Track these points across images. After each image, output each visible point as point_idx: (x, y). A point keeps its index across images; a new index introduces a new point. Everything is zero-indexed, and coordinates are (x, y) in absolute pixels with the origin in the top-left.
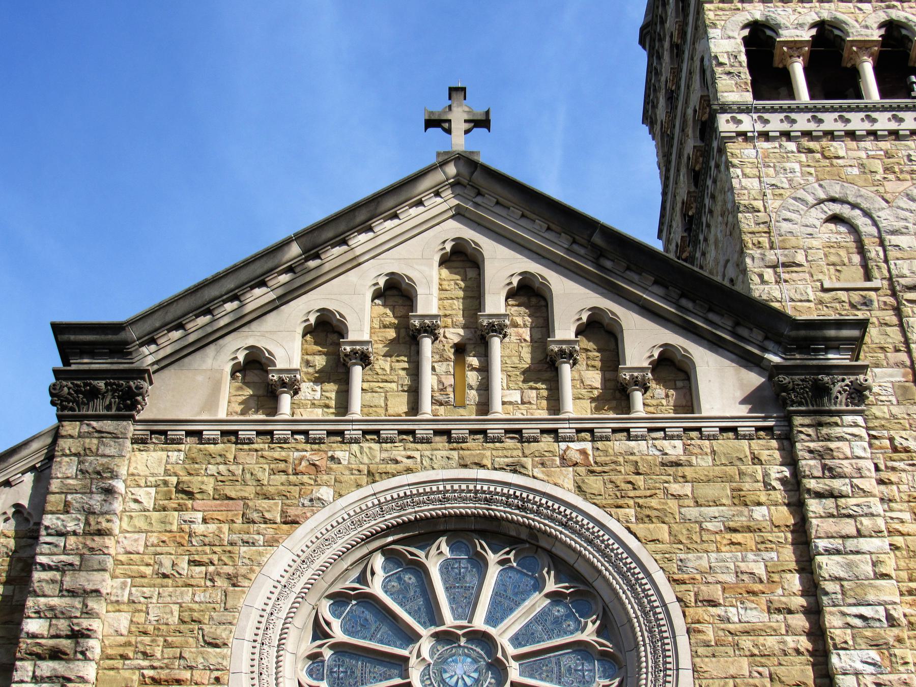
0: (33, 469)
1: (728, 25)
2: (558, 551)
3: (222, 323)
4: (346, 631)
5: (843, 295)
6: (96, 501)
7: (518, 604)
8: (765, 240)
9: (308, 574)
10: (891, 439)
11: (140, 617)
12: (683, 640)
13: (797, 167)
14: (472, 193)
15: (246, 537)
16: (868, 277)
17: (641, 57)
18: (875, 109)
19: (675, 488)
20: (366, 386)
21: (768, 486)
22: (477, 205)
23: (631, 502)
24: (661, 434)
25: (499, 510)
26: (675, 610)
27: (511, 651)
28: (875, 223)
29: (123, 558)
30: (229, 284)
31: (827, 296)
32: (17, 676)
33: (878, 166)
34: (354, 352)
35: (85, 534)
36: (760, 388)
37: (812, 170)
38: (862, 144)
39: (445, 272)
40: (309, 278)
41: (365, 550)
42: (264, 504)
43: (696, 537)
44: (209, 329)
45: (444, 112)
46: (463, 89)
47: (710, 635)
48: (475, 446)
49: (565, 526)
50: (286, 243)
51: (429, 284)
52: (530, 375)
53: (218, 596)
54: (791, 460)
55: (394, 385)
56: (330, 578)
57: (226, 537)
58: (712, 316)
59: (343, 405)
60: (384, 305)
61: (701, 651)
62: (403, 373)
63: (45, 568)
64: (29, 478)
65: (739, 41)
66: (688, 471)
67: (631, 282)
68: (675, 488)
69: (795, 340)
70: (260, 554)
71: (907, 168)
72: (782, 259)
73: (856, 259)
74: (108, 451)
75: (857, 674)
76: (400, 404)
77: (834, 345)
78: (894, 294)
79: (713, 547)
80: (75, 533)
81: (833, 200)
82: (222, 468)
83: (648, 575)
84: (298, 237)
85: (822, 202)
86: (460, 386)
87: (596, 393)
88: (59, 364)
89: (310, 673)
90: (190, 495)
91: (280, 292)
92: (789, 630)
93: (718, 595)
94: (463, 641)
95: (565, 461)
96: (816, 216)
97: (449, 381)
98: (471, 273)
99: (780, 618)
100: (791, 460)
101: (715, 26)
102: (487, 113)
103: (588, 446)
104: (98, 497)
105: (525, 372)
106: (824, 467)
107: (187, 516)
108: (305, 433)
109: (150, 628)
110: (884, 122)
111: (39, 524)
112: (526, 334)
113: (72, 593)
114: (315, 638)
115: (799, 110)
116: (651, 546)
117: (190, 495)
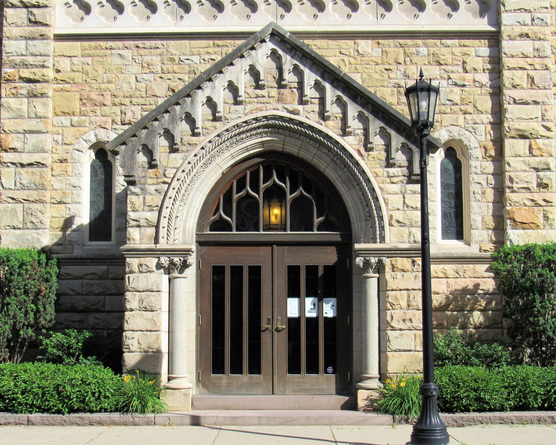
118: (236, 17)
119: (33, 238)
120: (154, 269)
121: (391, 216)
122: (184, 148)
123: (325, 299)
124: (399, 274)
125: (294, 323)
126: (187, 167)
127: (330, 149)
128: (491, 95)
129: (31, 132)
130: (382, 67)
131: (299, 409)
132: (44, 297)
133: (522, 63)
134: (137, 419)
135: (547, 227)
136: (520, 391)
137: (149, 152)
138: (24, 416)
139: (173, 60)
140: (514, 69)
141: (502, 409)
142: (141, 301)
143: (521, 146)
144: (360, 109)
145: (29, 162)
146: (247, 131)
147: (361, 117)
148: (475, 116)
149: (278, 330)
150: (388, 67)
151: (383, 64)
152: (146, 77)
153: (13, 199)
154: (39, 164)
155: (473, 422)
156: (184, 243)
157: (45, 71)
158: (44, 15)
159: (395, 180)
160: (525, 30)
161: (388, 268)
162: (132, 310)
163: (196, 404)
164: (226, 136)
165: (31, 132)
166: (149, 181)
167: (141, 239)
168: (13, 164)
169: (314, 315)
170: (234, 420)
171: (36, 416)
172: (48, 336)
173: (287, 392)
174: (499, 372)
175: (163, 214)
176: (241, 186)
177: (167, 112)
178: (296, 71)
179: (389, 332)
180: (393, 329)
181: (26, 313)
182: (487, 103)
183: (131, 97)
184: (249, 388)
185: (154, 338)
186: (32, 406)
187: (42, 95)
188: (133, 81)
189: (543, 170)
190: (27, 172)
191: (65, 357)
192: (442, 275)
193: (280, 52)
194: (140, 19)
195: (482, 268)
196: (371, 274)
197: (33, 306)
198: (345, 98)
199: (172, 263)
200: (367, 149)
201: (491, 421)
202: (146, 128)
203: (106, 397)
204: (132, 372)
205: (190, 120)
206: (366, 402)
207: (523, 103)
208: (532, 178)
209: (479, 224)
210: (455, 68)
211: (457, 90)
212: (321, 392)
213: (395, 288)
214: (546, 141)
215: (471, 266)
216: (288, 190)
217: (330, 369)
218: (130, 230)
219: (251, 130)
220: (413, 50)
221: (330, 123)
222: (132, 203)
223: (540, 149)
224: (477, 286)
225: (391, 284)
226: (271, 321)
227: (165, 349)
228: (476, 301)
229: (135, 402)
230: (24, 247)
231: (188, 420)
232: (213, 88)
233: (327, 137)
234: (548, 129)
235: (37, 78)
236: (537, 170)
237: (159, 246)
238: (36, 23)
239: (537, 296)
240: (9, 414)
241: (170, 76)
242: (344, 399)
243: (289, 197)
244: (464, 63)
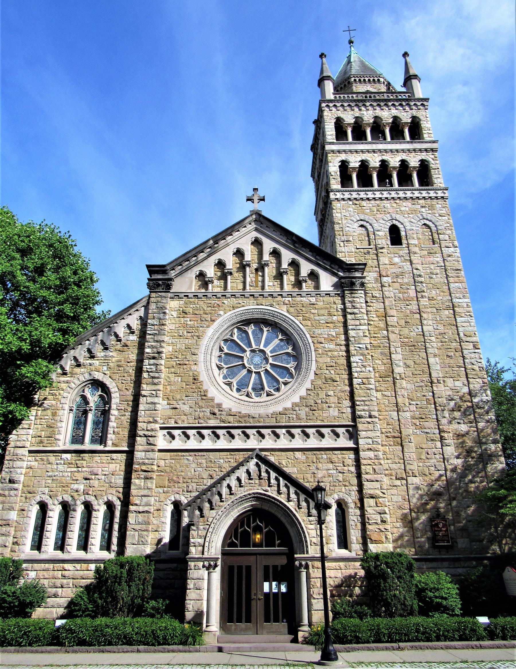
0: (144, 306)
1: (335, 162)
2: (282, 328)
3: (192, 263)
4: (228, 350)
5: (362, 250)
6: (161, 316)
7: (272, 342)
8: (341, 233)
9: (218, 335)
10: (372, 294)
11: (175, 347)
12: (313, 353)
13: (352, 209)
14: (260, 223)
15: (201, 325)
16: (370, 245)
17: (311, 154)
19: (313, 311)
20: (231, 281)
21: (337, 311)
22: (261, 227)
23: (301, 315)
24: (309, 296)
25: (267, 317)
26: (312, 344)
27: (270, 355)
28: (373, 228)
29: (169, 331)
30: (194, 252)
31: (358, 250)
32: (144, 364)
33: (375, 209)
34: (228, 272)
35: (160, 325)
36: (337, 282)
37: (356, 211)
38: (371, 202)
39: (252, 247)
40: (215, 250)
41: (232, 328)
42: (205, 316)
43: (318, 325)
44: (189, 266)
45: (252, 196)
46: (257, 189)
47: (320, 352)
48: (260, 298)
49: (284, 321)
50: (208, 241)
51: (248, 251)
52: (275, 278)
53: (195, 342)
54: (344, 303)
55: (239, 281)
56: (223, 335)
57: (196, 325)
58: (325, 261)
59: (225, 288)
60: (236, 257)
61: (318, 356)
62: (241, 277)
63: (150, 334)
64: (143, 308)
65: (338, 167)
66: (316, 306)
67: (303, 251)
68: (313, 311)
69: (346, 269)
70: (205, 330)
71: (383, 210)
72: (346, 239)
73: (367, 238)
74: (164, 302)
75: (357, 362)
76: (241, 286)
77: (357, 270)
78: (376, 250)
79: (322, 327)
80: (156, 325)
81: (361, 220)
82: (194, 306)
83: (305, 335)
84: (212, 238)
85: (358, 221)
86: (257, 281)
87: (293, 283)
88: (149, 277)
89: (219, 361)
90: (186, 313)
91: (208, 254)
92: (341, 351)
93: (323, 341)
94: (257, 352)
95: (284, 304)
96: (356, 225)
97: (254, 279)
98: (260, 247)
99: (338, 347)
100: (344, 303)
101: (331, 162)
102: (264, 197)
103: (290, 299)
104: (162, 315)
105: (274, 277)
106: (352, 305)
107: (186, 319)
108: (216, 295)
109: (178, 350)
110: (378, 195)
111: (147, 321)
112: (274, 265)
113: (157, 341)
114: (220, 351)
116: (306, 327)
117: (186, 313)
118: (240, 441)
119: (142, 549)
120: (201, 567)
121: (311, 541)
122: (217, 508)
123: (282, 583)
124: (316, 570)
125: (267, 595)
126: (218, 517)
127: (282, 508)
128: (357, 477)
129: (145, 496)
130: (306, 464)
131: (270, 642)
132: (148, 582)
133: (369, 462)
134: (191, 649)
135: (387, 542)
136: (376, 632)
137: (201, 510)
138: (135, 647)
139: (211, 461)
140: (366, 465)
141: (368, 642)
142: (195, 584)
143: (372, 502)
144: (295, 489)
145: (142, 510)
146: (245, 500)
147: (296, 493)
148: (350, 487)
149: (259, 599)
150: (309, 464)
151: (307, 463)
152: (199, 469)
153: (134, 529)
154: (147, 512)
155: (354, 650)
156: (215, 554)
157: (153, 466)
158: (154, 441)
159: (312, 523)
160: (370, 446)
161: (310, 567)
162: (190, 589)
163: (220, 640)
164: (236, 502)
165: (145, 496)
166: (201, 524)
167: (196, 552)
168: (135, 511)
169: (276, 591)
170: (238, 649)
171: (141, 647)
172: (148, 603)
173: (264, 633)
174: (366, 622)
175: (206, 540)
176: (242, 526)
177: (209, 491)
178: (267, 472)
179: (312, 600)
180: (314, 599)
181: (139, 590)
182: (355, 481)
183: (192, 479)
184: (245, 631)
185: (200, 604)
186: (140, 641)
187: (151, 478)
188: (193, 471)
189: (383, 514)
190: (141, 516)
191: (156, 614)
192: (339, 568)
193: (260, 463)
194: (197, 442)
195: (358, 564)
196: (303, 570)
197: (142, 586)
198: (289, 484)
199: (210, 565)
200: (299, 508)
201: (363, 649)
202: (200, 498)
203: (177, 636)
204: (189, 623)
205: (220, 495)
206: (303, 639)
207: (371, 481)
208: (378, 517)
209: (355, 541)
210: (340, 465)
211: (340, 475)
212: (281, 633)
213: (314, 577)
214: (383, 499)
215: (352, 563)
216: (264, 528)
217: (285, 620)
218: (191, 548)
219: (247, 499)
220: (320, 456)
221: (282, 496)
222: (193, 535)
223: (381, 503)
224: (356, 574)
225: (312, 575)
226: (256, 594)
227: (205, 610)
228: (356, 582)
229: (190, 640)
230: (138, 555)
231: (216, 649)
232: (230, 480)
233: (281, 502)
234: (384, 494)
235: (149, 470)
236: (380, 514)
237: (204, 556)
238: (150, 444)
239: (382, 581)
240: (128, 646)
241: (210, 469)
243: (265, 531)
244: (343, 462)
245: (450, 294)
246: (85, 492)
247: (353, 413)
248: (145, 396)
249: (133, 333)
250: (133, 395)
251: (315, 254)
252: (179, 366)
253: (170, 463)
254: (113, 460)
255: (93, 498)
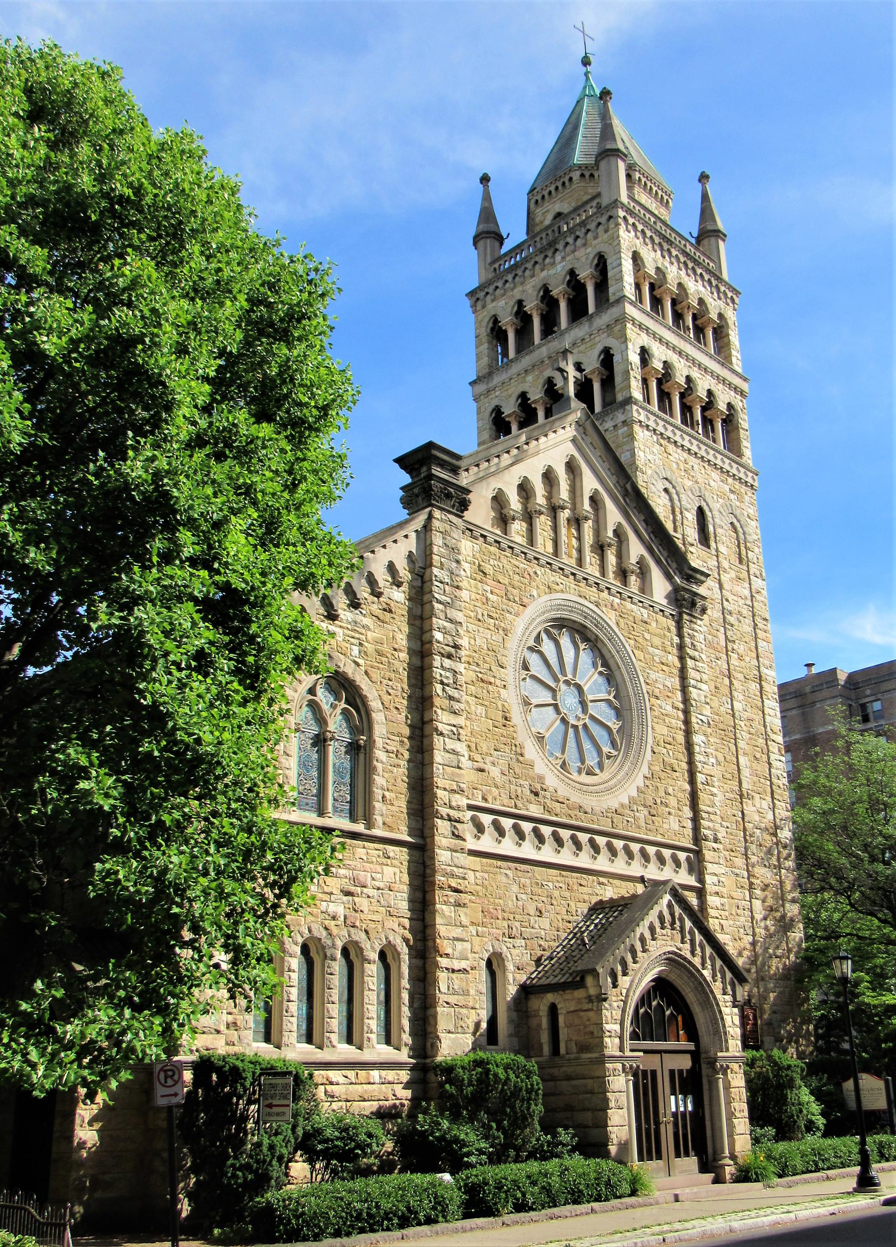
6: (454, 565)
18: (652, 413)
25: (588, 624)
69: (687, 575)
113: (451, 621)
115: (671, 425)
129: (458, 939)
165: (458, 939)
238: (458, 837)
242: (711, 1176)
245: (758, 657)
246: (348, 922)
247: (696, 828)
248: (442, 734)
249: (399, 585)
250: (409, 726)
251: (650, 529)
252: (482, 684)
253: (483, 878)
254: (389, 858)
255: (363, 935)
